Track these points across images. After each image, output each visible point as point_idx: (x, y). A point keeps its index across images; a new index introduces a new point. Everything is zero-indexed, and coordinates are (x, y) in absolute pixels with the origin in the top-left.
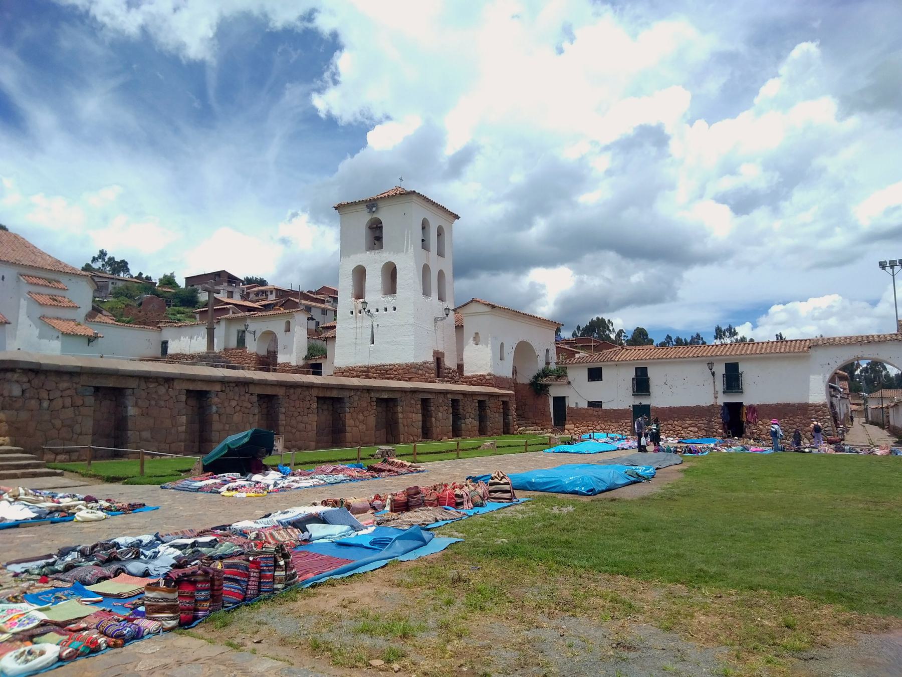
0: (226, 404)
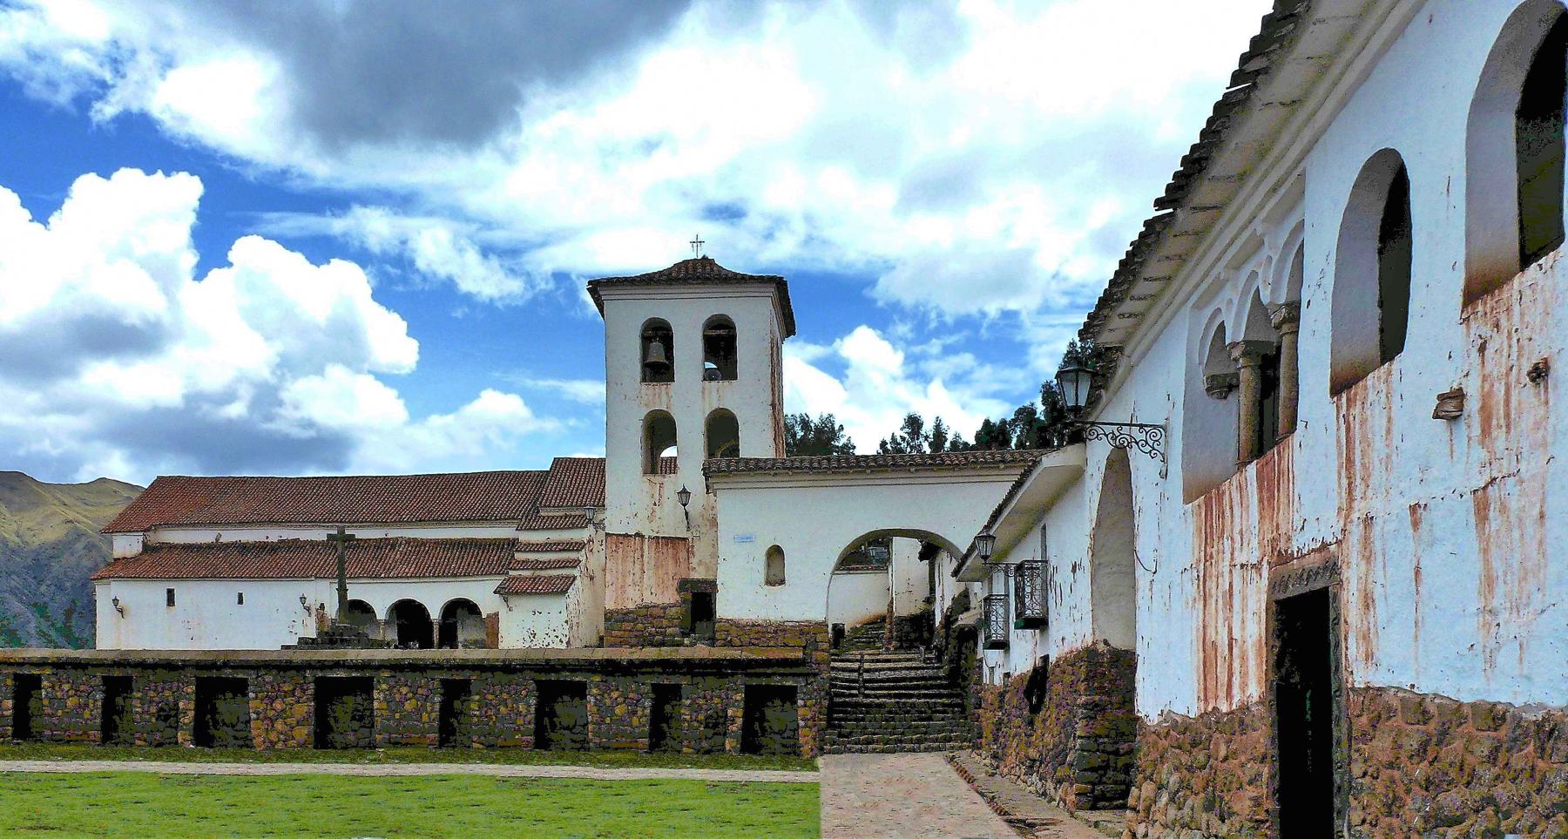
0: (57, 688)
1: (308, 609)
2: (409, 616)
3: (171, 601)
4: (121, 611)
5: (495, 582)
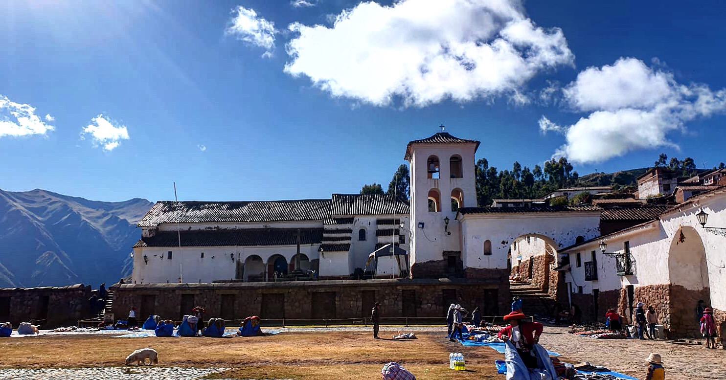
1: (233, 259)
2: (278, 259)
3: (170, 257)
4: (146, 262)
5: (316, 246)
